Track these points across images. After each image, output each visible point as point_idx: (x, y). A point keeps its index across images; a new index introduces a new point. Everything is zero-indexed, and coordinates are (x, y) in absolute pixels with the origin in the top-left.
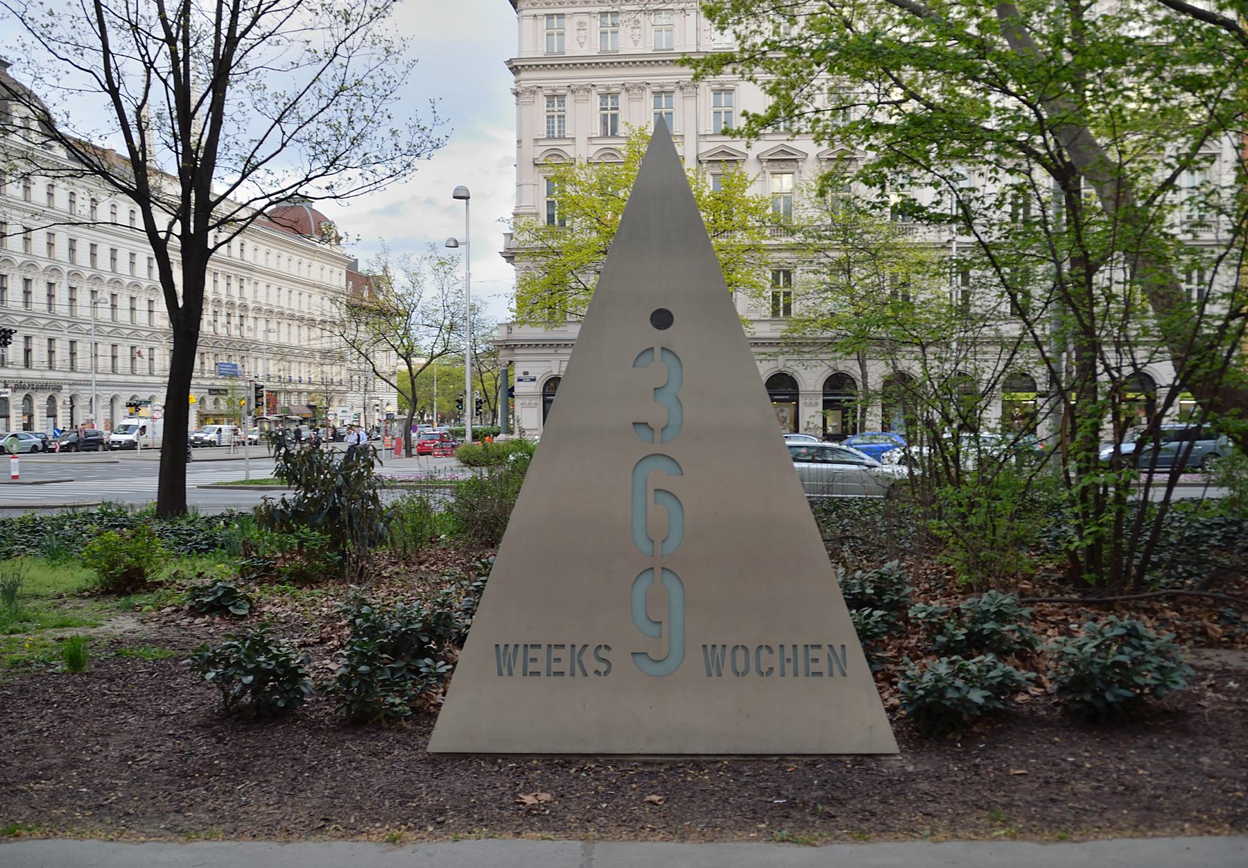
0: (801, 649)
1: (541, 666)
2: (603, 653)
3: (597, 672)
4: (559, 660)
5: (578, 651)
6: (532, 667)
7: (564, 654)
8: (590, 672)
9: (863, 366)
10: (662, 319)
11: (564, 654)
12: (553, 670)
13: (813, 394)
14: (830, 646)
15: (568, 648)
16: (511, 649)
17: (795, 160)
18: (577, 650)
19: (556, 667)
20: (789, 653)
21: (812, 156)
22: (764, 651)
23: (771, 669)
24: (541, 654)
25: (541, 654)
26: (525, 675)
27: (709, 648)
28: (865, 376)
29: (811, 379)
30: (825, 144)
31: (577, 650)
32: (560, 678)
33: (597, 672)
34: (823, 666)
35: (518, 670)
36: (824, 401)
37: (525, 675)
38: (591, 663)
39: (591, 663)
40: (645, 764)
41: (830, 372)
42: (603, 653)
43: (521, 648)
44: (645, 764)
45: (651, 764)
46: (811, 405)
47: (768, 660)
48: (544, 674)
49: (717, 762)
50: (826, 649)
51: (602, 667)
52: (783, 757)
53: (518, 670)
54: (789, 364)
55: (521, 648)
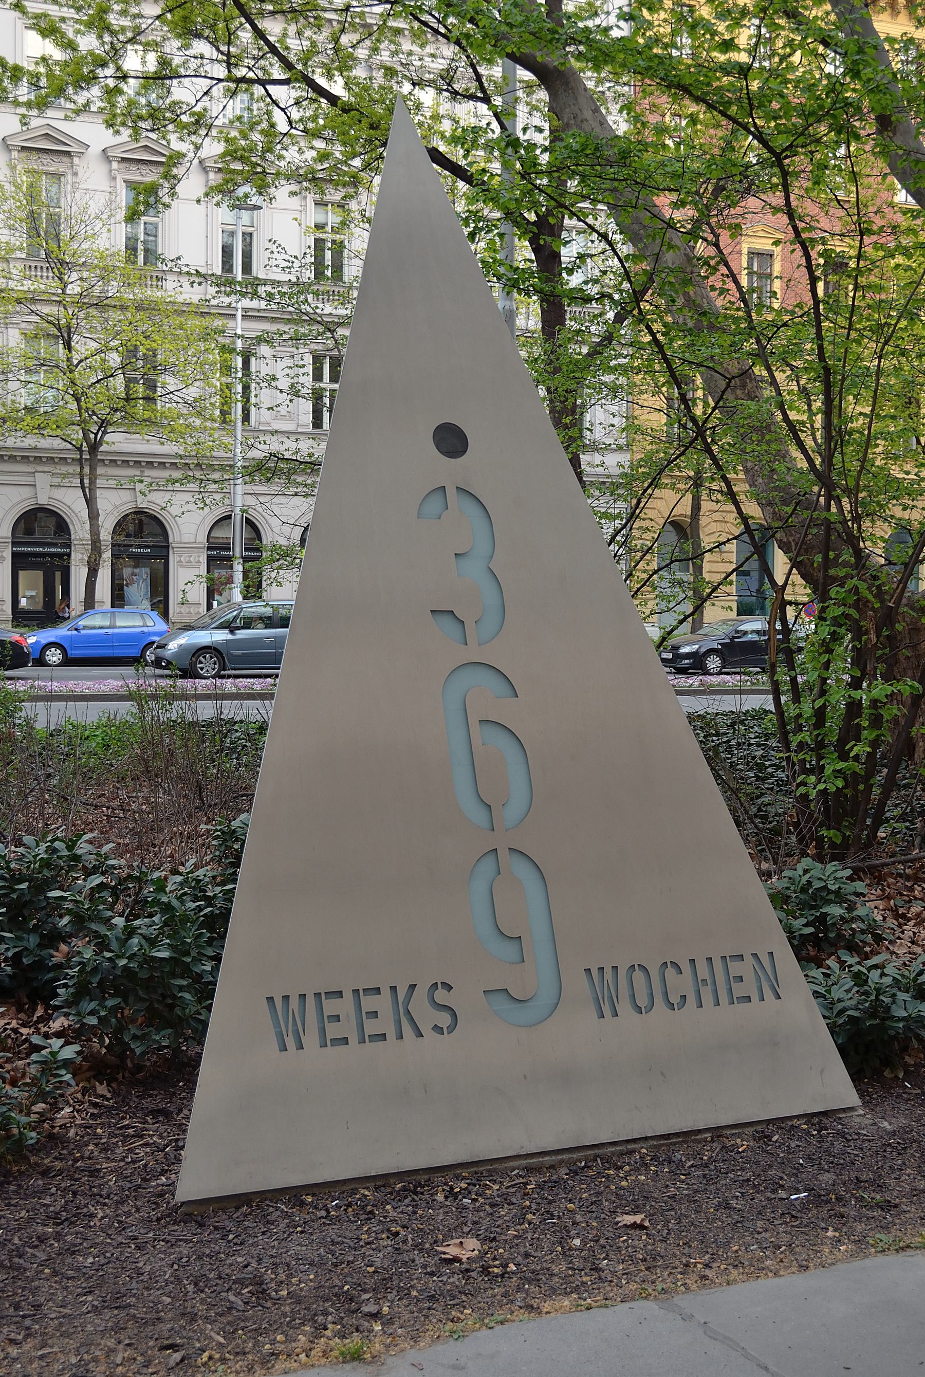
0: (718, 964)
1: (347, 1028)
2: (441, 996)
3: (438, 1029)
4: (337, 1018)
5: (402, 999)
6: (333, 1031)
7: (382, 1003)
8: (425, 1029)
9: (90, 502)
10: (451, 440)
11: (382, 1003)
12: (367, 1032)
13: (189, 548)
14: (755, 955)
15: (386, 992)
16: (294, 1003)
17: (68, 153)
18: (402, 993)
19: (371, 1027)
20: (703, 971)
21: (95, 149)
22: (670, 972)
23: (684, 997)
24: (344, 1007)
25: (344, 1007)
26: (324, 1045)
27: (595, 973)
28: (93, 515)
29: (188, 522)
30: (126, 133)
31: (402, 993)
32: (344, 1048)
33: (438, 1029)
34: (748, 987)
35: (311, 1039)
36: (14, 554)
37: (324, 1045)
38: (426, 1016)
39: (426, 1016)
40: (537, 1169)
41: (127, 508)
42: (441, 996)
43: (311, 1001)
44: (529, 1170)
45: (537, 1169)
46: (189, 565)
47: (680, 984)
48: (353, 1040)
49: (632, 1152)
50: (749, 959)
51: (444, 1020)
52: (717, 1132)
53: (311, 1039)
54: (59, 494)
55: (311, 1001)
